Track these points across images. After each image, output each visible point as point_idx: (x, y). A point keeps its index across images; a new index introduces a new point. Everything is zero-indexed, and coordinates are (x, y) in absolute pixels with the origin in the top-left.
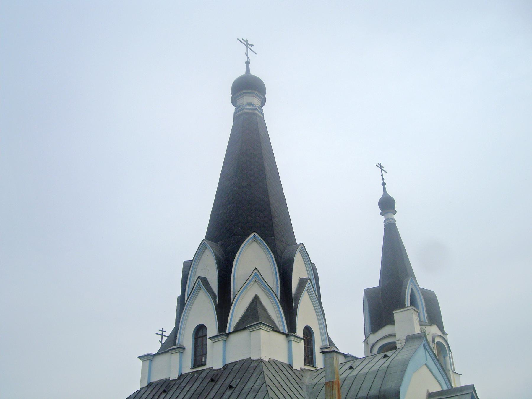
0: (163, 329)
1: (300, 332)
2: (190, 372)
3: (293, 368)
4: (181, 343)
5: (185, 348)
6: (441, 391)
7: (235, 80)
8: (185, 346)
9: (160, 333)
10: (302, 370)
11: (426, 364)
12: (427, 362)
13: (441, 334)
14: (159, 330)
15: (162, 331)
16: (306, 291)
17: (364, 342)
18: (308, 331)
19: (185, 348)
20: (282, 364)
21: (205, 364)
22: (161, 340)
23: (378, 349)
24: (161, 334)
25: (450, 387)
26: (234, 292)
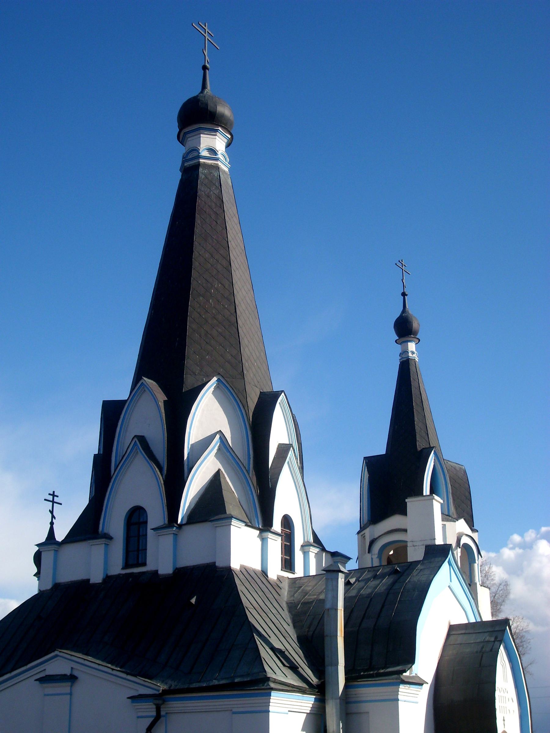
0: (54, 492)
1: (277, 526)
2: (120, 574)
3: (268, 577)
4: (105, 531)
5: (113, 538)
6: (467, 623)
7: (182, 104)
8: (112, 534)
9: (51, 498)
10: (278, 579)
11: (449, 587)
13: (469, 532)
14: (50, 494)
15: (53, 495)
17: (358, 533)
18: (287, 522)
19: (113, 538)
20: (255, 571)
21: (144, 564)
22: (51, 510)
24: (52, 500)
25: (479, 620)
26: (188, 465)
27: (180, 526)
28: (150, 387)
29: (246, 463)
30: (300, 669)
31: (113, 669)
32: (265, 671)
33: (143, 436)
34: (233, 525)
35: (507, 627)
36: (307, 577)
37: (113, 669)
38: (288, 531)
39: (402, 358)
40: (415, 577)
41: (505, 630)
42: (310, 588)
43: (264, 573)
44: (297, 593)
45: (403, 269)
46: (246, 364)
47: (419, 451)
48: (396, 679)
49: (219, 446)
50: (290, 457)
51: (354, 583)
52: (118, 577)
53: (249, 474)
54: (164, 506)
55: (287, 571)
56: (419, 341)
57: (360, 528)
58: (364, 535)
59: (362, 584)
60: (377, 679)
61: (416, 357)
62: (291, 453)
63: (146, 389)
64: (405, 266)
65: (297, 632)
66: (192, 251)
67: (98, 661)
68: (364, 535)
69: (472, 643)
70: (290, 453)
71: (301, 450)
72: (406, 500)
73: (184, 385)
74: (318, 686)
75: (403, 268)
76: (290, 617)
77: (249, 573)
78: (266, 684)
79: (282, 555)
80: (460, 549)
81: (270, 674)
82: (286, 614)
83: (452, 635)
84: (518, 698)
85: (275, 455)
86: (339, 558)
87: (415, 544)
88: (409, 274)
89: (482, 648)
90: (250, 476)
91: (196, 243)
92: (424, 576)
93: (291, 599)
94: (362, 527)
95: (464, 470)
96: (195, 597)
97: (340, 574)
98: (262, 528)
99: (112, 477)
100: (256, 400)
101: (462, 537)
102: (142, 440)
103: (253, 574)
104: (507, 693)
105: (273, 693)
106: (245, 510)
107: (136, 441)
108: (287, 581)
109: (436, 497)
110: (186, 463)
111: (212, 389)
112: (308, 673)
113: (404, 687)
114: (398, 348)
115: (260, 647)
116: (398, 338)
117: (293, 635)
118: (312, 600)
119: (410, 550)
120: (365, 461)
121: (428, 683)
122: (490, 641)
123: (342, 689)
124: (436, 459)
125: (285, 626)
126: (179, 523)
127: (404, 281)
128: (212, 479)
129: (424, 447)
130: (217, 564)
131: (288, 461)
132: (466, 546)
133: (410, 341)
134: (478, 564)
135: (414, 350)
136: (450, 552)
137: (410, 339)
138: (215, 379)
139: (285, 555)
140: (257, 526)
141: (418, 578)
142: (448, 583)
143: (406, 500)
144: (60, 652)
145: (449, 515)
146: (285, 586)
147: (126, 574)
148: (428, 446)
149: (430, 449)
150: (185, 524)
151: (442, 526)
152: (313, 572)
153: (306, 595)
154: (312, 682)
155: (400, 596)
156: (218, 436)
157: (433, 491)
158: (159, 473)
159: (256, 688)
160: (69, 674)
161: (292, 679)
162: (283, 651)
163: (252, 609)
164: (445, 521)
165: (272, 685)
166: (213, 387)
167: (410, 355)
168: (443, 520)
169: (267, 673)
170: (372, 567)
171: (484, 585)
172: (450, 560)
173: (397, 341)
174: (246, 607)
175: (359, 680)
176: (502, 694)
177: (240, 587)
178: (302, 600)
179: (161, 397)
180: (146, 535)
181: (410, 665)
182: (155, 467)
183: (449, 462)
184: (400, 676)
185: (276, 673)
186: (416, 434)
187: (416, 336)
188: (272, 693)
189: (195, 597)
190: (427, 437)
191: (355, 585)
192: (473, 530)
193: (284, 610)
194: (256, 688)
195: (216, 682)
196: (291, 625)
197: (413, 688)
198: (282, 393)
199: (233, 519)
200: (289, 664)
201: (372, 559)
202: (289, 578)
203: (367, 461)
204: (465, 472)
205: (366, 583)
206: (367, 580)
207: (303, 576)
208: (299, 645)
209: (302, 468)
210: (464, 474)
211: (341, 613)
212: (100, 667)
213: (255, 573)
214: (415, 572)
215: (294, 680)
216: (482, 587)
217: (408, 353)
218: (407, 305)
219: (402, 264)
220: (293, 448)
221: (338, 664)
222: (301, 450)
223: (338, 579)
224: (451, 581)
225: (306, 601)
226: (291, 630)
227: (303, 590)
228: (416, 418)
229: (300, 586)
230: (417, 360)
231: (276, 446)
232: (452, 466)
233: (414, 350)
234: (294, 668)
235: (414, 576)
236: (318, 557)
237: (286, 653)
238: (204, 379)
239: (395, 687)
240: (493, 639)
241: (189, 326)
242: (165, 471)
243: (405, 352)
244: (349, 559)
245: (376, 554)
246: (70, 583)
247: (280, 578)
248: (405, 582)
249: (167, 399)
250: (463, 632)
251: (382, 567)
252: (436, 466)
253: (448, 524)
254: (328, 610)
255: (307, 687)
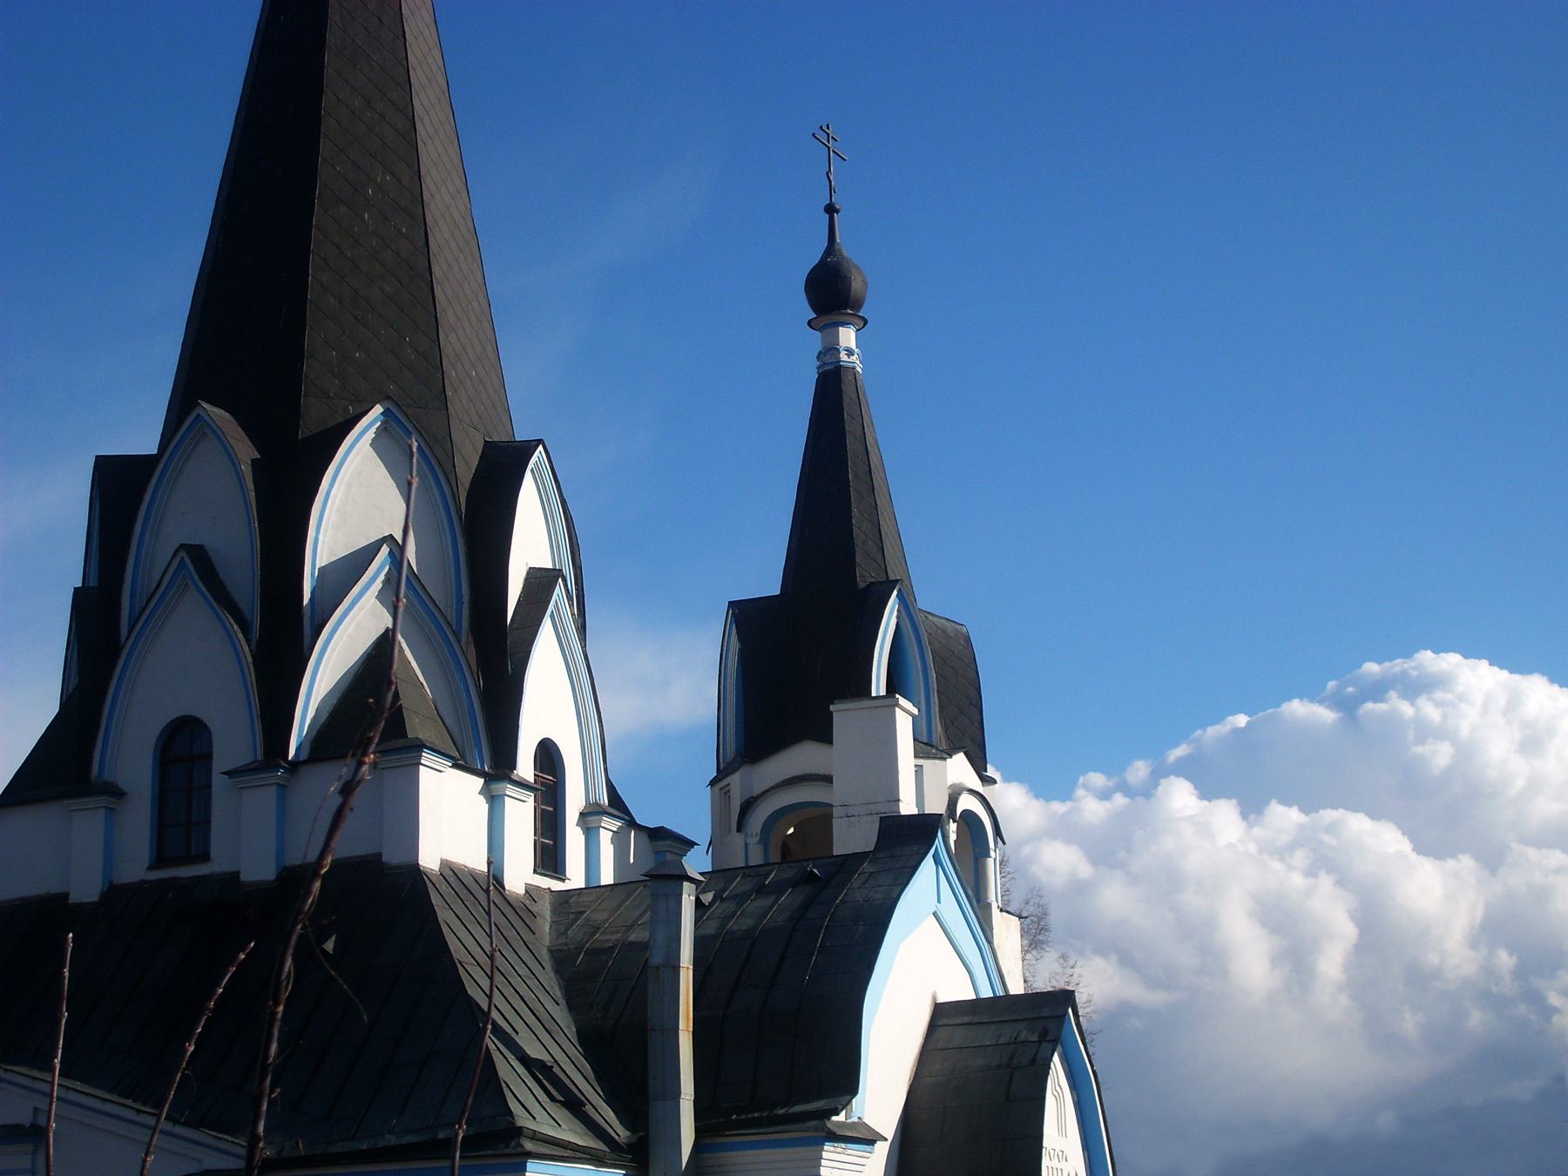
1: (525, 767)
2: (143, 882)
3: (504, 888)
4: (107, 777)
5: (126, 794)
11: (935, 914)
12: (938, 904)
13: (975, 784)
16: (549, 619)
17: (713, 783)
18: (548, 754)
19: (126, 794)
20: (473, 874)
21: (205, 857)
23: (763, 820)
25: (1001, 993)
26: (312, 618)
27: (294, 766)
28: (219, 427)
29: (451, 614)
30: (588, 1107)
31: (139, 1111)
32: (511, 1113)
33: (202, 546)
34: (425, 766)
35: (1070, 1010)
36: (593, 889)
37: (139, 1111)
38: (551, 778)
39: (824, 364)
40: (857, 891)
41: (1064, 1016)
42: (604, 916)
43: (495, 877)
44: (574, 927)
45: (829, 148)
46: (451, 374)
47: (861, 590)
48: (816, 1129)
49: (388, 573)
50: (556, 602)
51: (711, 904)
52: (140, 888)
53: (459, 640)
54: (255, 716)
55: (546, 876)
56: (866, 322)
57: (717, 772)
58: (727, 789)
59: (730, 906)
60: (771, 1130)
61: (858, 362)
62: (559, 592)
63: (209, 433)
64: (836, 140)
65: (576, 1022)
66: (319, 91)
67: (98, 1093)
68: (727, 789)
69: (990, 1046)
70: (557, 590)
71: (580, 585)
72: (832, 708)
73: (301, 423)
74: (629, 1145)
75: (830, 145)
76: (559, 984)
77: (460, 880)
78: (513, 1144)
79: (535, 835)
80: (956, 824)
81: (522, 1120)
82: (549, 977)
83: (940, 1026)
84: (1088, 1171)
85: (520, 597)
86: (668, 842)
87: (851, 811)
88: (845, 160)
89: (1012, 1057)
90: (462, 644)
91: (329, 72)
92: (879, 889)
93: (560, 942)
94: (722, 768)
95: (965, 636)
96: (334, 938)
97: (686, 885)
98: (490, 771)
99: (123, 648)
100: (475, 462)
101: (960, 794)
102: (198, 556)
103: (469, 882)
104: (1066, 1161)
105: (532, 1165)
106: (450, 728)
107: (182, 558)
108: (547, 897)
109: (902, 701)
110: (307, 614)
111: (371, 434)
112: (607, 1115)
113: (832, 1149)
114: (815, 340)
115: (497, 1057)
116: (815, 316)
117: (568, 1027)
118: (611, 945)
119: (838, 825)
120: (731, 612)
121: (886, 1140)
122: (1030, 1042)
123: (690, 1151)
124: (902, 609)
125: (550, 1005)
126: (290, 757)
127: (831, 178)
128: (371, 653)
129: (873, 580)
130: (385, 859)
131: (552, 612)
132: (969, 816)
133: (844, 324)
134: (995, 859)
135: (853, 345)
136: (939, 834)
137: (847, 319)
138: (378, 410)
139: (543, 835)
140: (479, 767)
141: (864, 896)
142: (932, 904)
143: (832, 708)
144: (6, 1070)
145: (929, 742)
146: (545, 909)
147: (158, 881)
148: (882, 578)
149: (891, 585)
150: (304, 763)
151: (914, 769)
152: (607, 877)
153: (596, 933)
154: (617, 1137)
155: (821, 936)
156: (385, 550)
157: (893, 686)
158: (241, 636)
159: (489, 1152)
160: (28, 1124)
161: (570, 1132)
162: (549, 1064)
163: (471, 966)
164: (922, 758)
165: (529, 1146)
166: (373, 429)
167: (843, 356)
168: (916, 756)
169: (516, 1118)
170: (747, 867)
171: (1009, 909)
172: (938, 853)
173: (812, 324)
174: (460, 962)
175: (727, 1133)
176: (1055, 1163)
177: (443, 915)
178: (585, 945)
179: (246, 452)
180: (209, 786)
181: (848, 1097)
182: (232, 621)
183: (930, 617)
184: (825, 1125)
185: (535, 1118)
186: (856, 548)
187: (858, 311)
188: (528, 1164)
189: (334, 938)
190: (880, 556)
191: (713, 909)
192: (987, 780)
193: (544, 969)
194: (489, 1152)
195: (392, 1140)
196: (562, 1001)
197: (852, 1153)
198: (538, 446)
199: (425, 750)
200: (563, 1097)
201: (746, 845)
202: (553, 889)
203: (737, 611)
204: (968, 640)
205: (739, 905)
206: (741, 899)
207: (583, 886)
208: (583, 1049)
209: (582, 629)
210: (965, 645)
211: (688, 976)
212: (108, 1107)
213: (476, 881)
214: (857, 881)
215: (580, 1135)
216: (1004, 914)
217: (840, 353)
218: (837, 236)
219: (828, 135)
220: (565, 580)
221: (680, 1095)
222: (579, 581)
223: (682, 895)
224: (939, 902)
225: (597, 946)
226: (561, 1014)
227: (588, 920)
228: (855, 510)
229: (582, 909)
230: (860, 370)
231: (524, 574)
232: (936, 626)
233: (853, 345)
234: (574, 1105)
235: (854, 889)
236: (619, 839)
237: (556, 1070)
238: (351, 408)
239: (814, 1148)
240: (1035, 1038)
241: (313, 276)
242: (256, 634)
243: (831, 349)
244: (691, 844)
245: (757, 834)
246: (17, 903)
247: (531, 891)
248: (834, 902)
249: (259, 457)
250: (966, 1020)
251: (812, 862)
252: (903, 628)
253: (927, 764)
254: (657, 968)
255: (608, 1150)
